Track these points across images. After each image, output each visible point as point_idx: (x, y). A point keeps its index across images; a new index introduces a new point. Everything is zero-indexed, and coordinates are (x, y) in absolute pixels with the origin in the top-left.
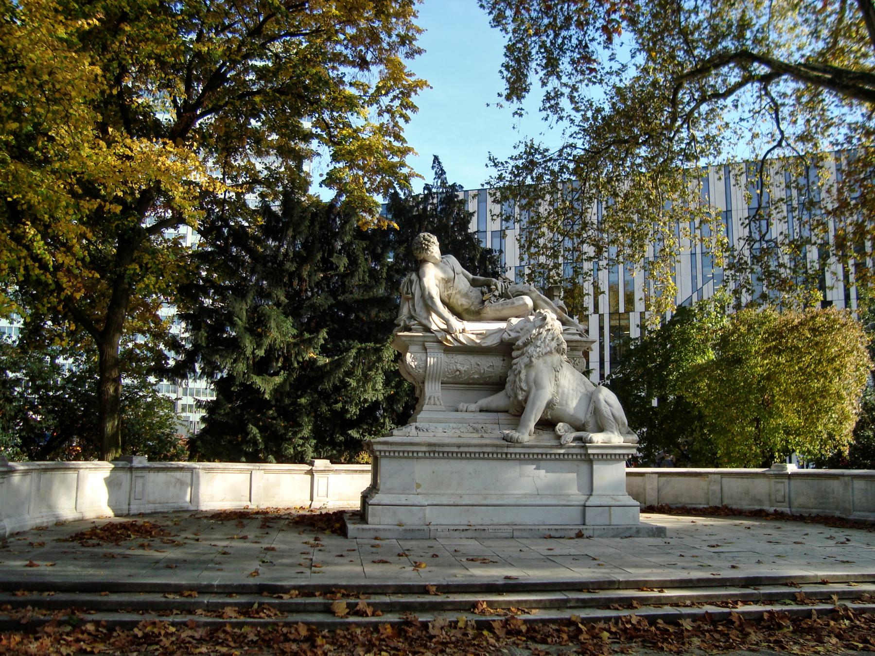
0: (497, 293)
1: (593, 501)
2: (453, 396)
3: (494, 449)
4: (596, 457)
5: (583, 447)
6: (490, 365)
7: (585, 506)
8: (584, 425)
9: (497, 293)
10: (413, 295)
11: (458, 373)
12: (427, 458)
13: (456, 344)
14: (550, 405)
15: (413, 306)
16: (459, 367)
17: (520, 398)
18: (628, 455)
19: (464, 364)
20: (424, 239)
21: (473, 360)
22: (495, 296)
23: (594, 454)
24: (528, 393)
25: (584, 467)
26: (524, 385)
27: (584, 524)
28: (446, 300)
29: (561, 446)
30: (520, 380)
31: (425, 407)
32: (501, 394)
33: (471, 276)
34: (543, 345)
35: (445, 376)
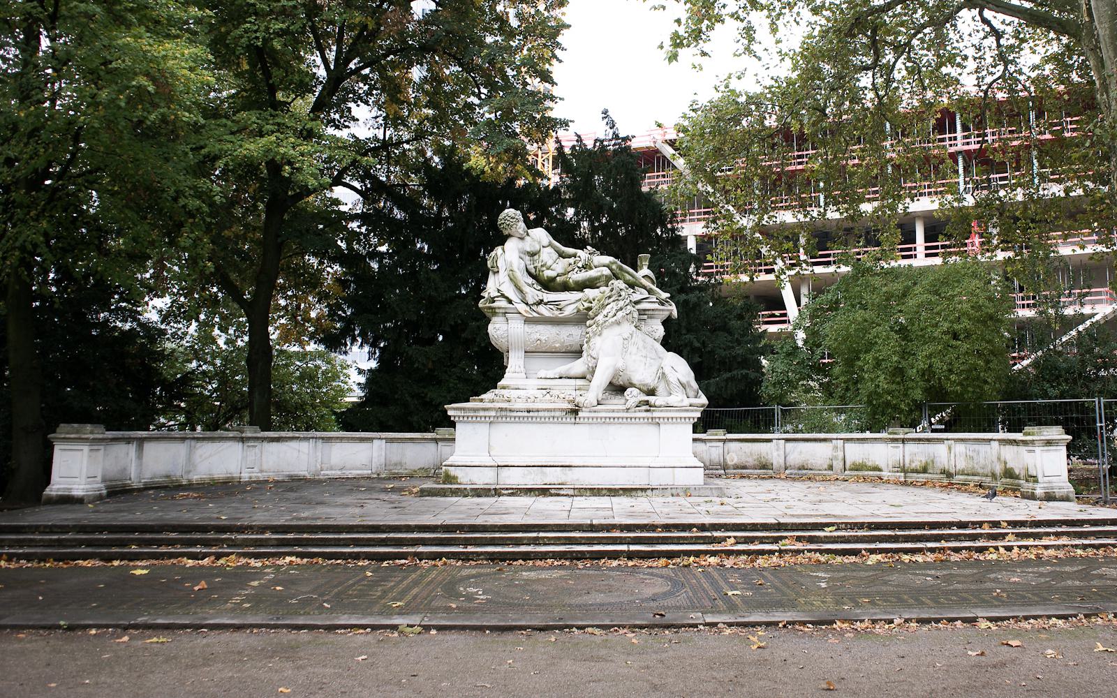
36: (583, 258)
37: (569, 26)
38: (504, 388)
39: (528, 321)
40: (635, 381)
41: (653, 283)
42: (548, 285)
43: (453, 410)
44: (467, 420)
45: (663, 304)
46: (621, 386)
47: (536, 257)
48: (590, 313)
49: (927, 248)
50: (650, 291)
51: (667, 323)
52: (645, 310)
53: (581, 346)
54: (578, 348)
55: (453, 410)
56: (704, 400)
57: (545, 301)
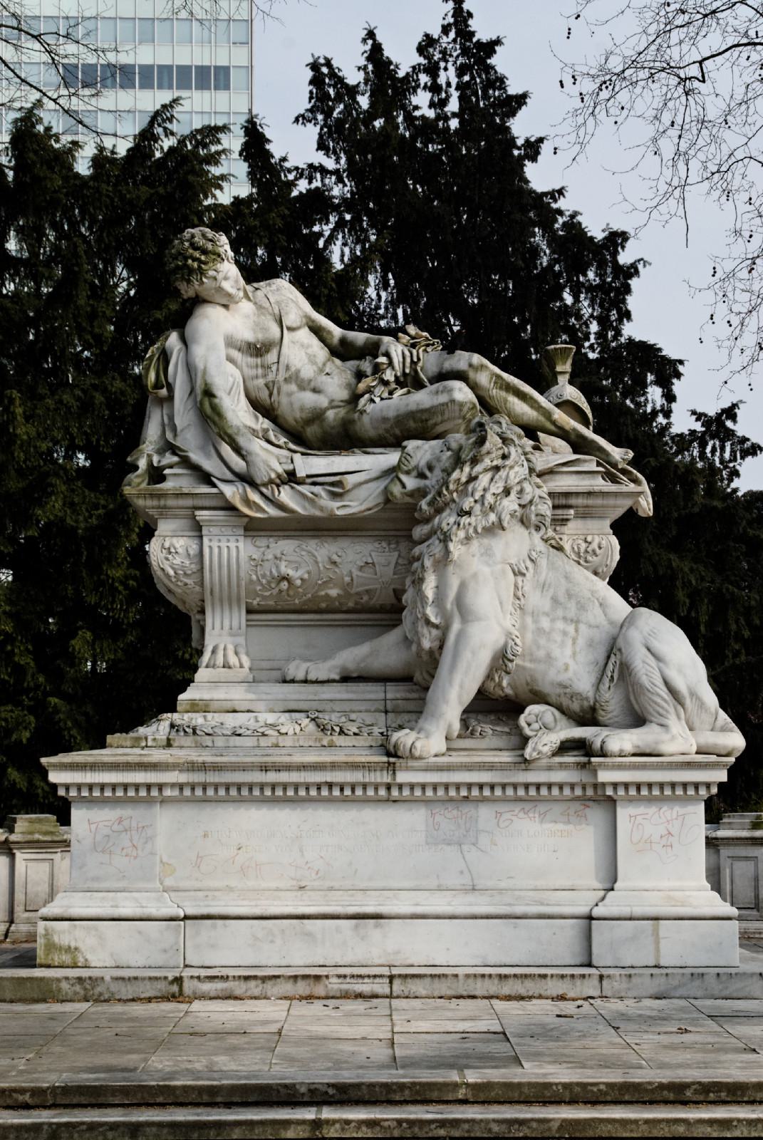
0: (389, 376)
1: (613, 905)
2: (280, 641)
3: (357, 776)
4: (621, 792)
5: (583, 766)
6: (353, 564)
7: (590, 918)
8: (593, 709)
9: (389, 376)
10: (170, 388)
11: (284, 585)
12: (188, 800)
13: (273, 512)
14: (502, 659)
15: (171, 418)
16: (285, 569)
17: (426, 644)
18: (708, 785)
19: (297, 561)
20: (194, 246)
21: (323, 550)
22: (386, 383)
23: (615, 786)
24: (444, 629)
25: (597, 815)
26: (431, 613)
27: (590, 965)
28: (264, 395)
29: (525, 763)
30: (423, 598)
31: (202, 674)
32: (393, 637)
33: (337, 332)
34: (478, 507)
35: (251, 593)
36: (397, 360)
37: (498, 42)
38: (195, 707)
39: (253, 528)
40: (546, 688)
41: (586, 422)
42: (307, 434)
43: (62, 773)
44: (100, 796)
45: (614, 480)
46: (507, 699)
47: (271, 357)
48: (424, 504)
49: (247, 620)
50: (580, 445)
51: (626, 526)
52: (567, 495)
53: (398, 594)
54: (389, 599)
55: (62, 773)
56: (736, 741)
57: (301, 473)
